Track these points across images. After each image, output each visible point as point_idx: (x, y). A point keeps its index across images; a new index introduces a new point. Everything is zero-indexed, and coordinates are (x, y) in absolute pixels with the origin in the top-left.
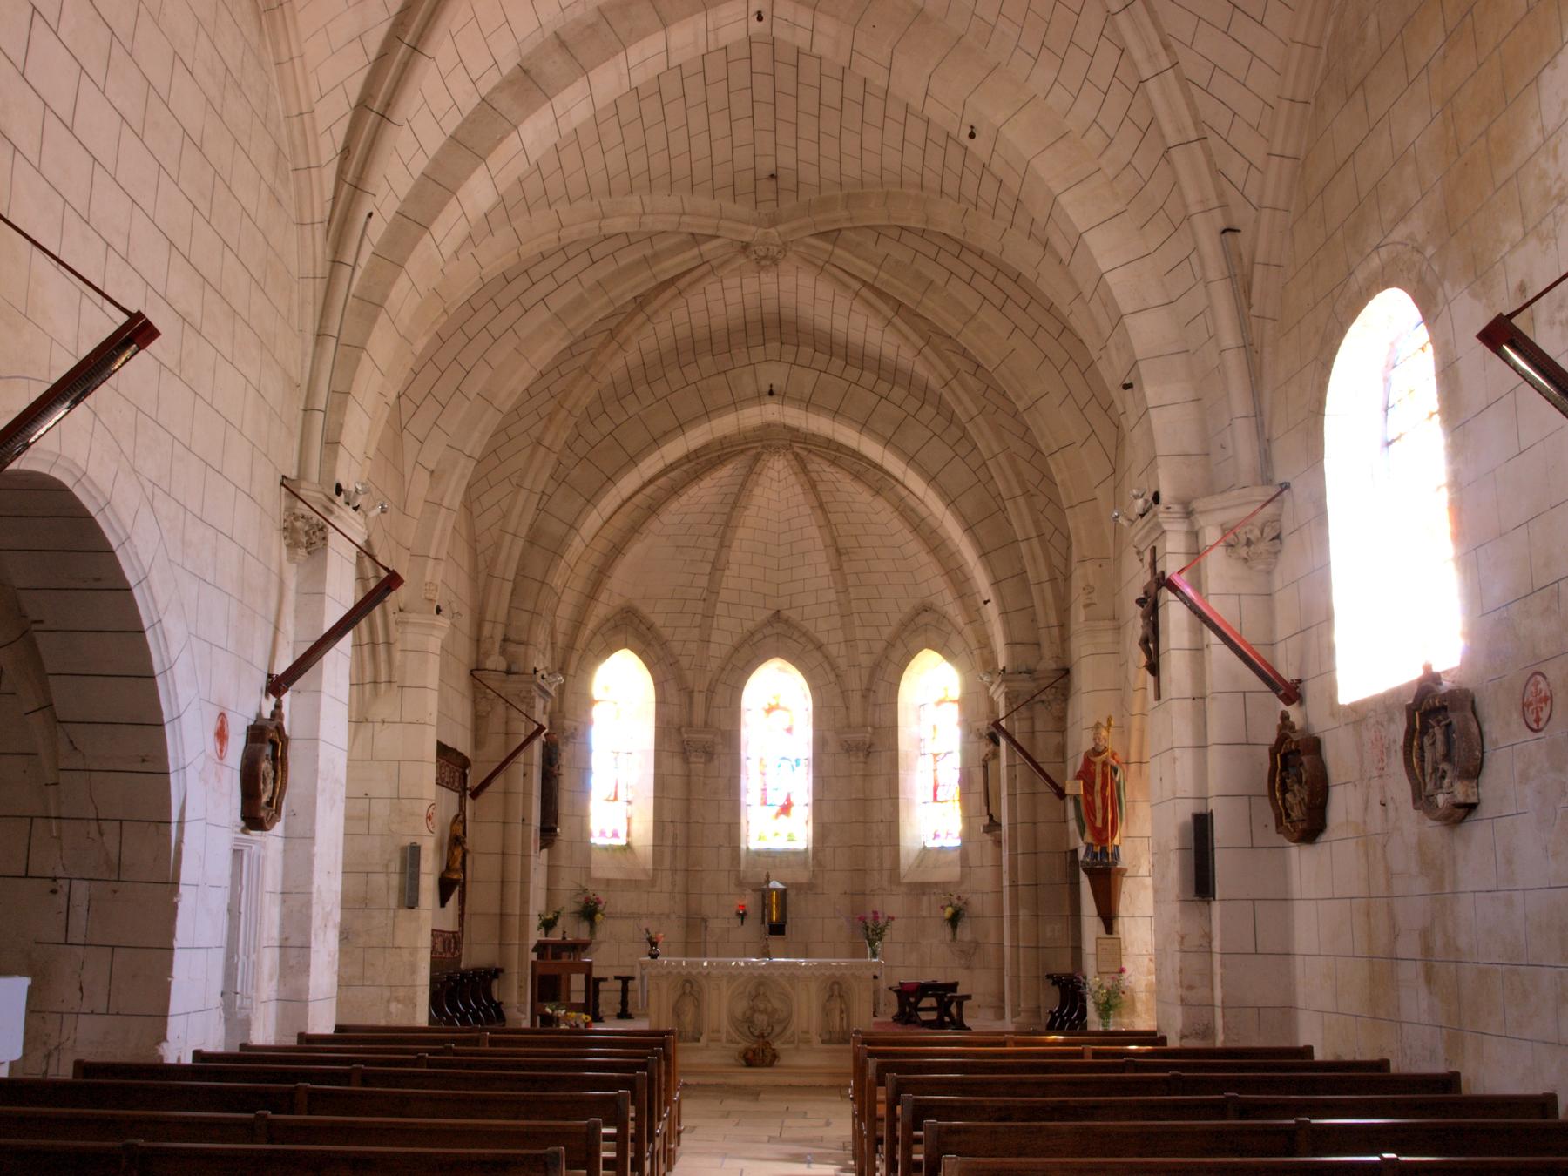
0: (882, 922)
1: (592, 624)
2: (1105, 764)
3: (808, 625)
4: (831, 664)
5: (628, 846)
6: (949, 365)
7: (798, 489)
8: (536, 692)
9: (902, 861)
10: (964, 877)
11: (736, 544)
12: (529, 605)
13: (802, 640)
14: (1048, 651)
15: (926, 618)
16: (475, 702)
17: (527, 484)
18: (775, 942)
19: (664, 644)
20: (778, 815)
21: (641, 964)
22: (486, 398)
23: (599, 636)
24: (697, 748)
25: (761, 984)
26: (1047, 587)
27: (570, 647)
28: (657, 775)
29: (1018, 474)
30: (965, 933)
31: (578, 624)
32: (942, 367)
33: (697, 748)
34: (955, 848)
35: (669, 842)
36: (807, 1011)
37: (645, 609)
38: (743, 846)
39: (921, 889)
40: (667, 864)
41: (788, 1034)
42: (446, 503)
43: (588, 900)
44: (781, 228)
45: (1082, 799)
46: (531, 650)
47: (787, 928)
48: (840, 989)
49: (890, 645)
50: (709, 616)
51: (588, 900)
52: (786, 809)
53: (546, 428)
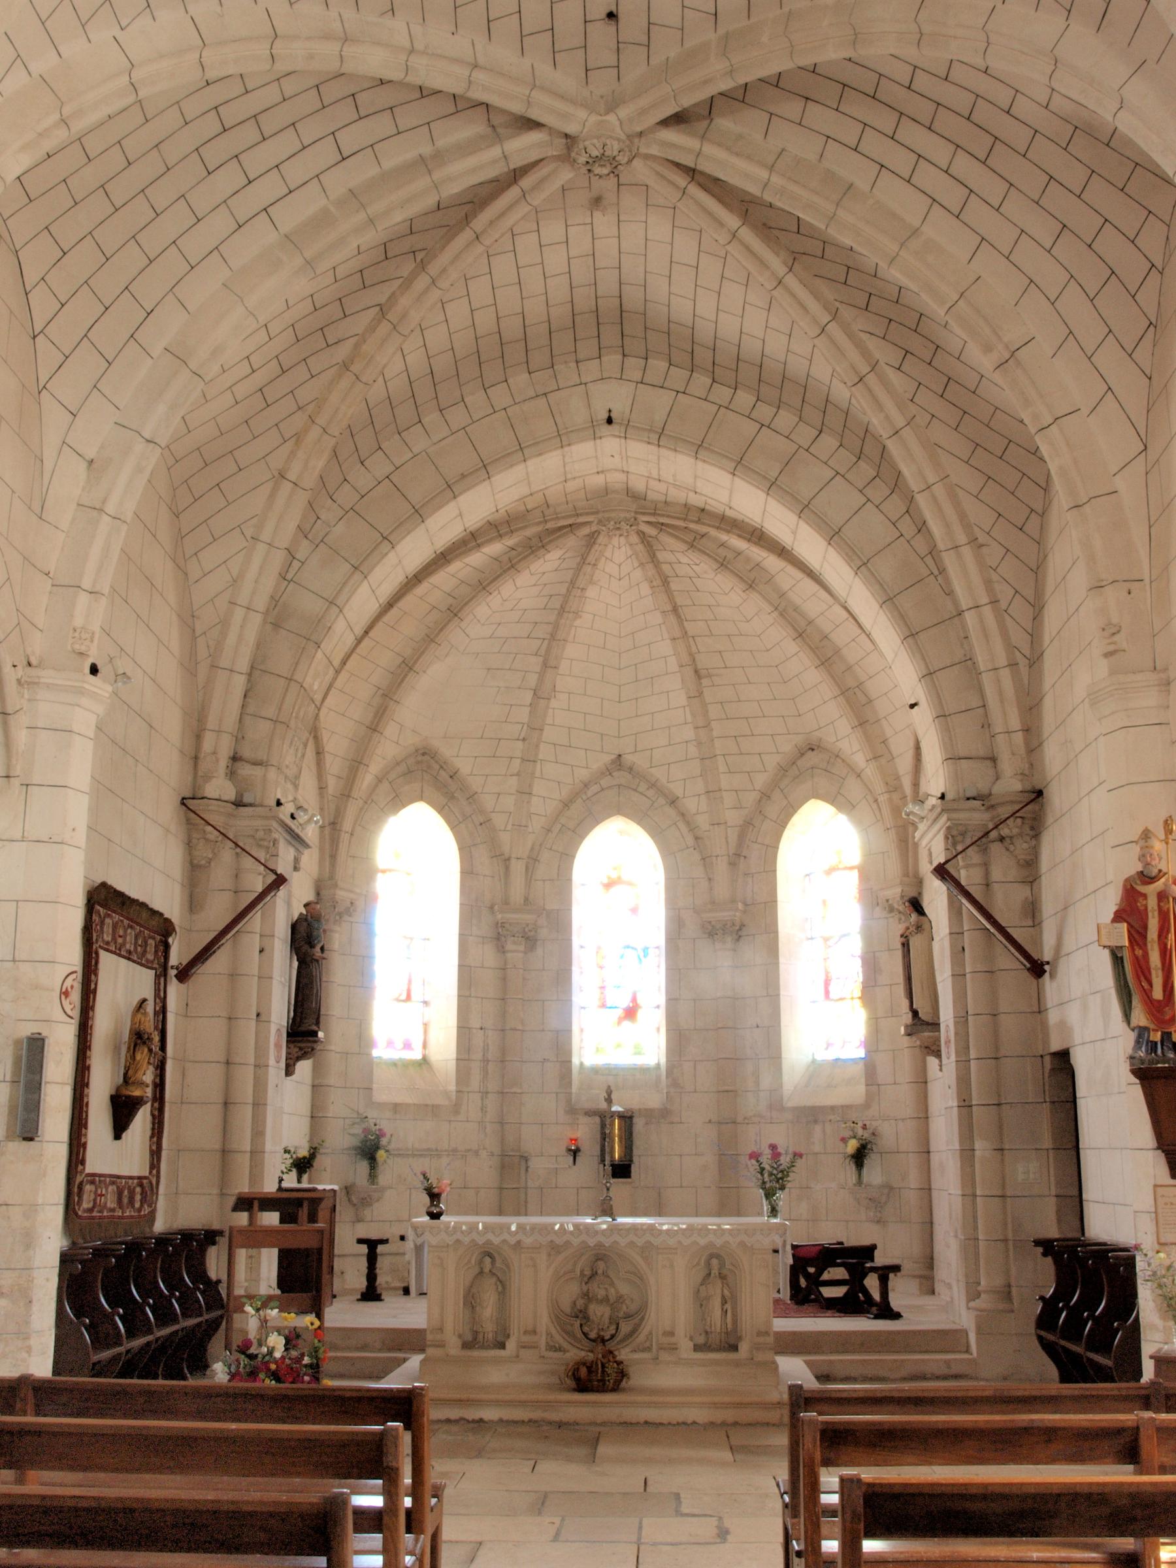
0: (785, 1161)
1: (375, 767)
2: (1162, 896)
3: (658, 773)
4: (688, 823)
5: (425, 1061)
6: (865, 353)
7: (645, 589)
8: (280, 835)
9: (786, 1078)
10: (870, 1098)
11: (564, 666)
12: (270, 712)
13: (651, 793)
14: (1009, 765)
15: (812, 758)
16: (189, 845)
17: (266, 536)
18: (619, 1188)
19: (472, 797)
20: (620, 1021)
21: (415, 1228)
22: (178, 355)
23: (385, 786)
24: (515, 937)
25: (599, 1257)
26: (1005, 674)
27: (346, 795)
28: (462, 967)
29: (963, 517)
30: (874, 1173)
31: (356, 764)
32: (853, 354)
33: (515, 937)
34: (854, 1061)
35: (478, 1056)
36: (671, 1304)
37: (446, 751)
38: (575, 1061)
39: (812, 1115)
40: (475, 1082)
41: (641, 1337)
42: (110, 508)
43: (366, 1131)
44: (623, 112)
45: (1126, 955)
46: (272, 774)
47: (634, 1169)
48: (722, 1265)
49: (765, 796)
50: (529, 760)
51: (366, 1131)
52: (630, 1013)
53: (293, 454)
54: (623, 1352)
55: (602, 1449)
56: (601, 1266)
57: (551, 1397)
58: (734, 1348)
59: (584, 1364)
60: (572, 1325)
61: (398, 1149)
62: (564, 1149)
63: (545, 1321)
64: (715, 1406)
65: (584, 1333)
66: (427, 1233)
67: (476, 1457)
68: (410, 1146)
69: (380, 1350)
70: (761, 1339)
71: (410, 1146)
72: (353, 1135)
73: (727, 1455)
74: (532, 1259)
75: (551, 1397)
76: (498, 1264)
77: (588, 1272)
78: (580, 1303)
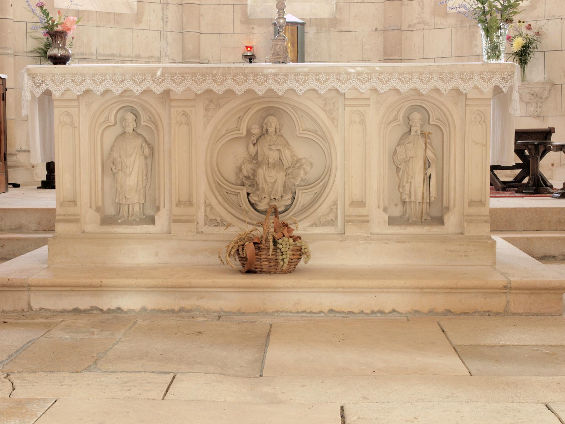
41: (323, 207)
48: (426, 120)
54: (301, 225)
55: (277, 353)
56: (272, 123)
57: (209, 281)
58: (440, 221)
59: (251, 240)
60: (238, 194)
61: (82, 54)
62: (240, 56)
63: (202, 189)
64: (422, 290)
65: (252, 204)
66: (47, 82)
67: (88, 369)
68: (94, 51)
69: (36, 231)
70: (473, 210)
71: (94, 51)
72: (37, 39)
73: (452, 363)
74: (185, 114)
75: (209, 281)
76: (144, 120)
77: (256, 131)
78: (247, 169)
